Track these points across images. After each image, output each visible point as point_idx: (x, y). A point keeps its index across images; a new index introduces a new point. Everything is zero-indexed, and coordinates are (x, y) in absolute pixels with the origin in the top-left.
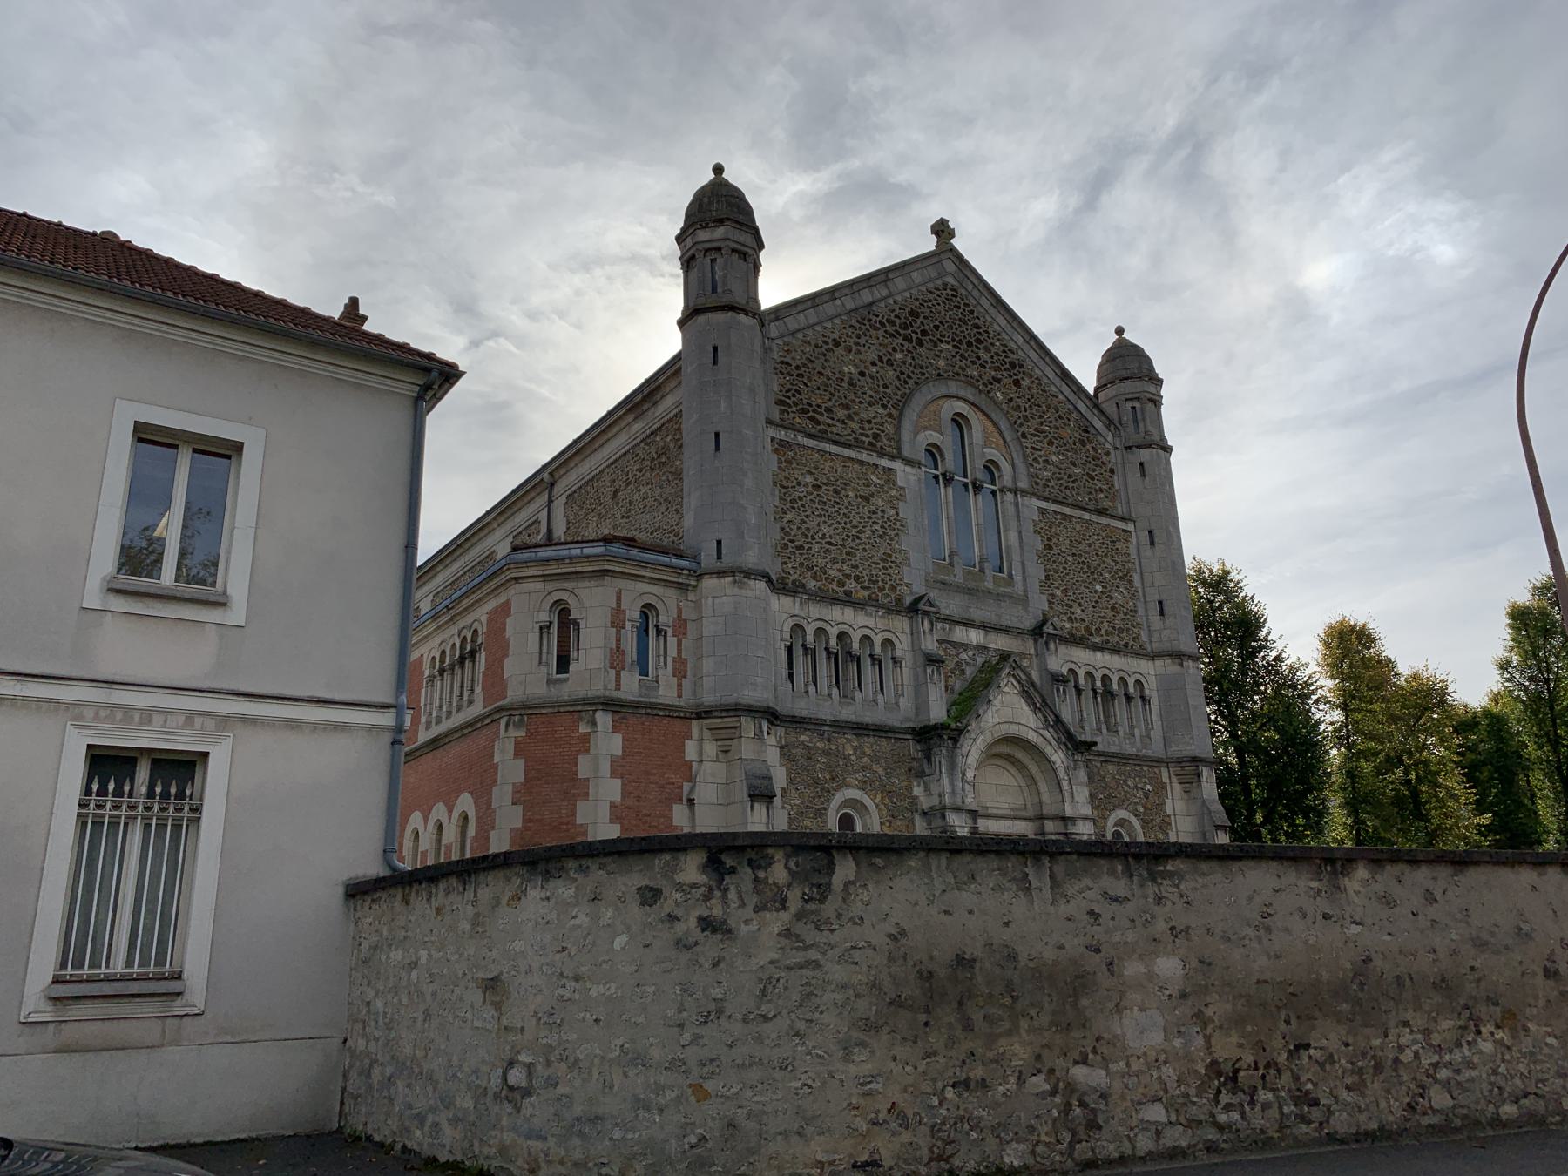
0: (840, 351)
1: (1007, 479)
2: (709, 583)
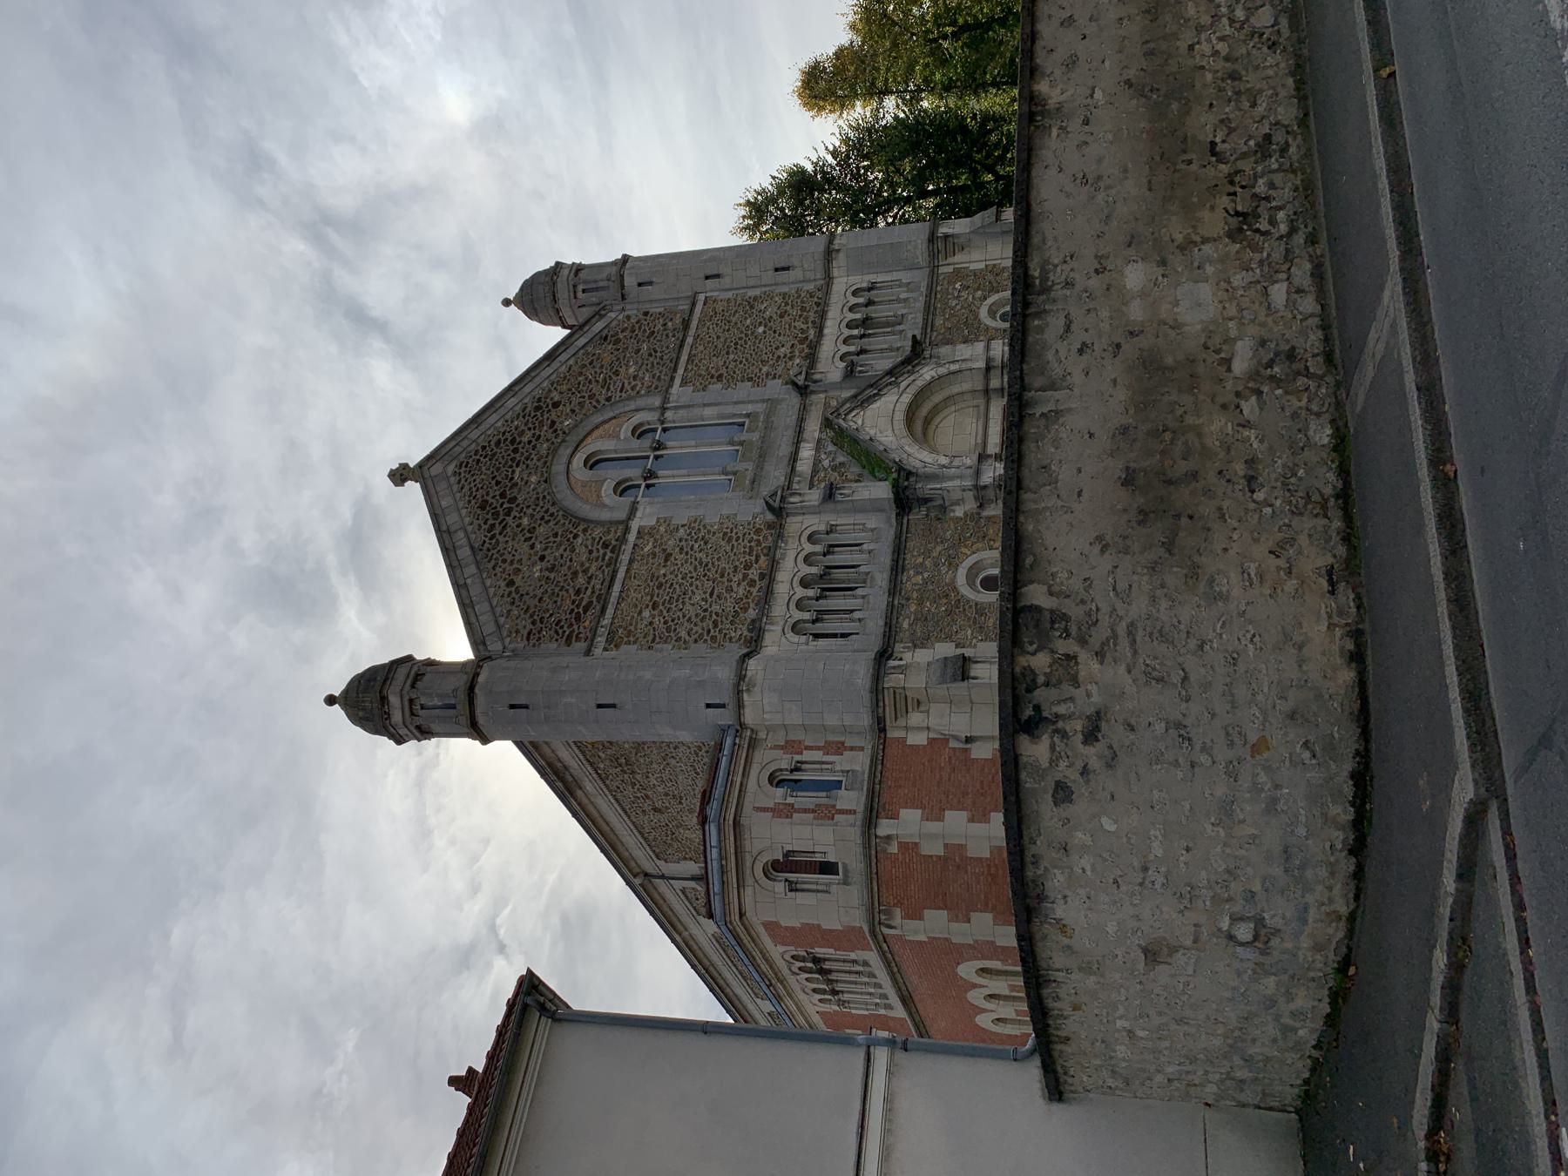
0: (518, 581)
2: (749, 717)
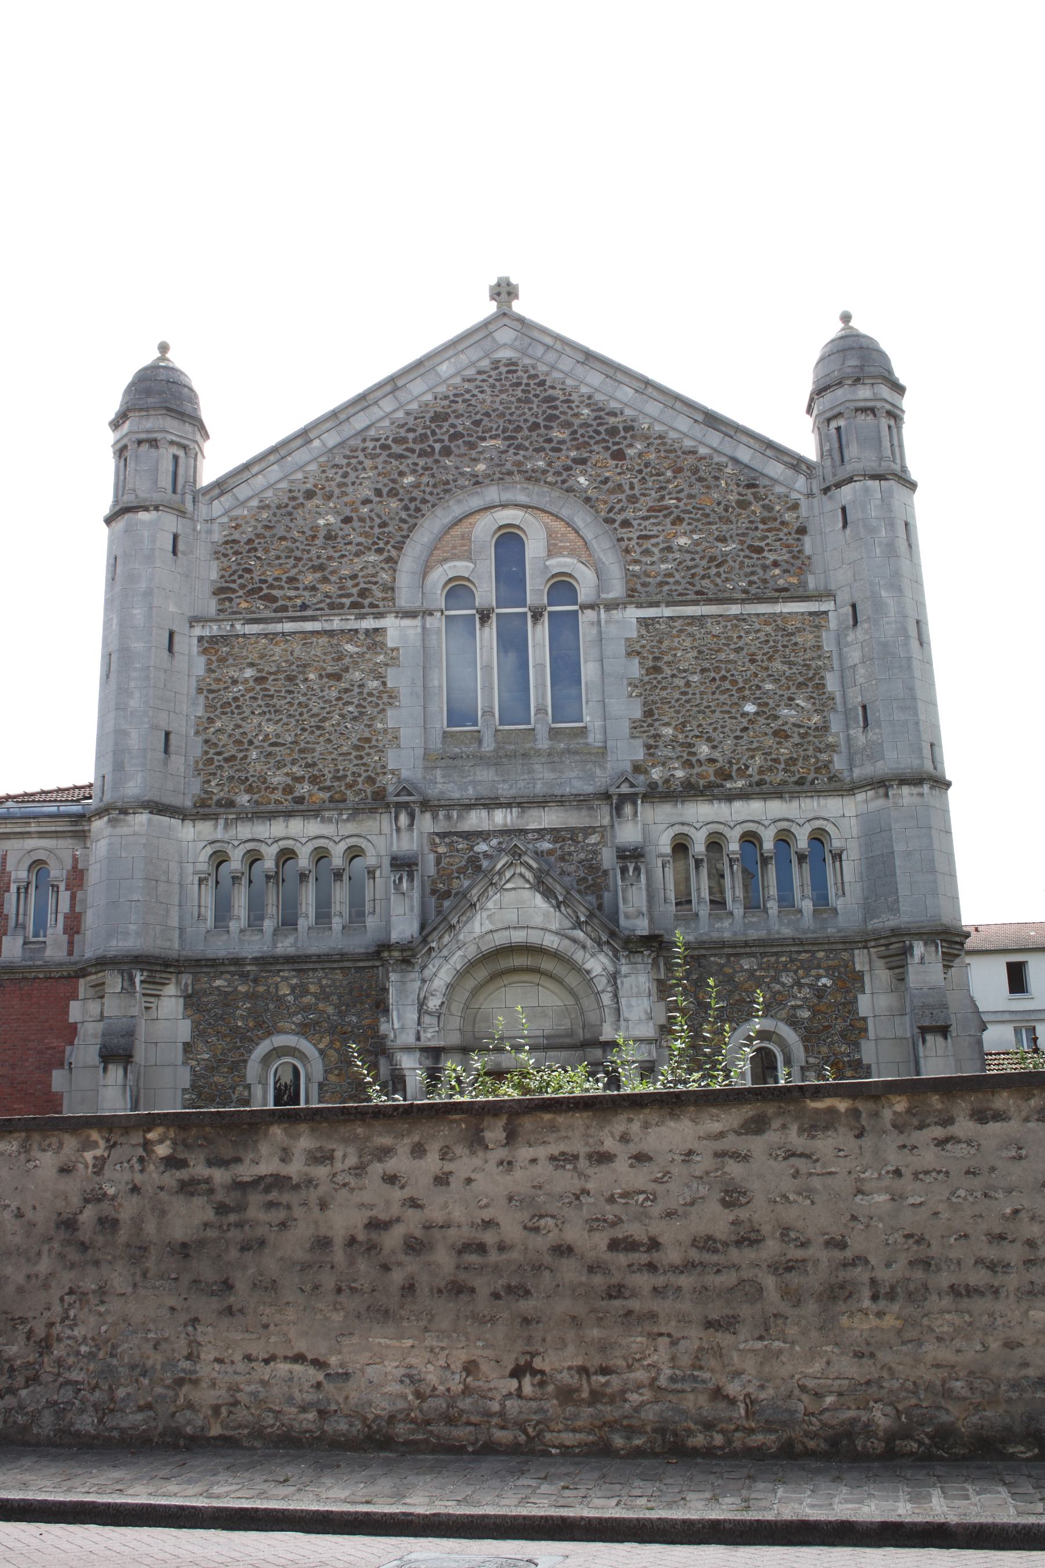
1: (585, 592)
